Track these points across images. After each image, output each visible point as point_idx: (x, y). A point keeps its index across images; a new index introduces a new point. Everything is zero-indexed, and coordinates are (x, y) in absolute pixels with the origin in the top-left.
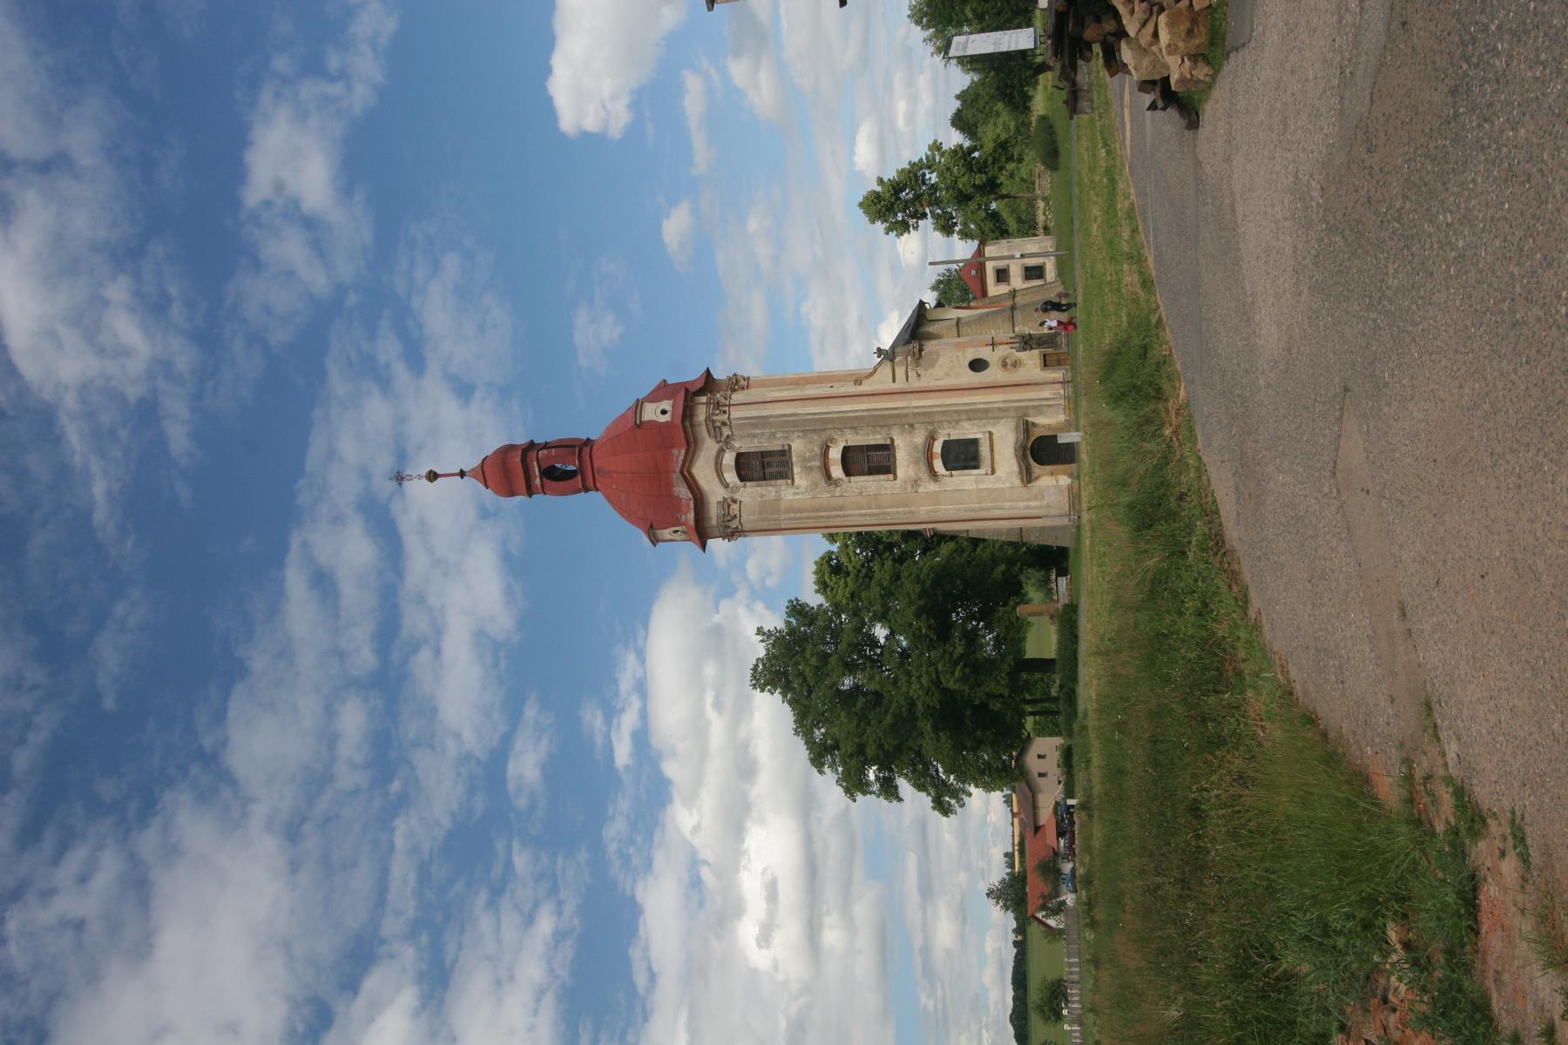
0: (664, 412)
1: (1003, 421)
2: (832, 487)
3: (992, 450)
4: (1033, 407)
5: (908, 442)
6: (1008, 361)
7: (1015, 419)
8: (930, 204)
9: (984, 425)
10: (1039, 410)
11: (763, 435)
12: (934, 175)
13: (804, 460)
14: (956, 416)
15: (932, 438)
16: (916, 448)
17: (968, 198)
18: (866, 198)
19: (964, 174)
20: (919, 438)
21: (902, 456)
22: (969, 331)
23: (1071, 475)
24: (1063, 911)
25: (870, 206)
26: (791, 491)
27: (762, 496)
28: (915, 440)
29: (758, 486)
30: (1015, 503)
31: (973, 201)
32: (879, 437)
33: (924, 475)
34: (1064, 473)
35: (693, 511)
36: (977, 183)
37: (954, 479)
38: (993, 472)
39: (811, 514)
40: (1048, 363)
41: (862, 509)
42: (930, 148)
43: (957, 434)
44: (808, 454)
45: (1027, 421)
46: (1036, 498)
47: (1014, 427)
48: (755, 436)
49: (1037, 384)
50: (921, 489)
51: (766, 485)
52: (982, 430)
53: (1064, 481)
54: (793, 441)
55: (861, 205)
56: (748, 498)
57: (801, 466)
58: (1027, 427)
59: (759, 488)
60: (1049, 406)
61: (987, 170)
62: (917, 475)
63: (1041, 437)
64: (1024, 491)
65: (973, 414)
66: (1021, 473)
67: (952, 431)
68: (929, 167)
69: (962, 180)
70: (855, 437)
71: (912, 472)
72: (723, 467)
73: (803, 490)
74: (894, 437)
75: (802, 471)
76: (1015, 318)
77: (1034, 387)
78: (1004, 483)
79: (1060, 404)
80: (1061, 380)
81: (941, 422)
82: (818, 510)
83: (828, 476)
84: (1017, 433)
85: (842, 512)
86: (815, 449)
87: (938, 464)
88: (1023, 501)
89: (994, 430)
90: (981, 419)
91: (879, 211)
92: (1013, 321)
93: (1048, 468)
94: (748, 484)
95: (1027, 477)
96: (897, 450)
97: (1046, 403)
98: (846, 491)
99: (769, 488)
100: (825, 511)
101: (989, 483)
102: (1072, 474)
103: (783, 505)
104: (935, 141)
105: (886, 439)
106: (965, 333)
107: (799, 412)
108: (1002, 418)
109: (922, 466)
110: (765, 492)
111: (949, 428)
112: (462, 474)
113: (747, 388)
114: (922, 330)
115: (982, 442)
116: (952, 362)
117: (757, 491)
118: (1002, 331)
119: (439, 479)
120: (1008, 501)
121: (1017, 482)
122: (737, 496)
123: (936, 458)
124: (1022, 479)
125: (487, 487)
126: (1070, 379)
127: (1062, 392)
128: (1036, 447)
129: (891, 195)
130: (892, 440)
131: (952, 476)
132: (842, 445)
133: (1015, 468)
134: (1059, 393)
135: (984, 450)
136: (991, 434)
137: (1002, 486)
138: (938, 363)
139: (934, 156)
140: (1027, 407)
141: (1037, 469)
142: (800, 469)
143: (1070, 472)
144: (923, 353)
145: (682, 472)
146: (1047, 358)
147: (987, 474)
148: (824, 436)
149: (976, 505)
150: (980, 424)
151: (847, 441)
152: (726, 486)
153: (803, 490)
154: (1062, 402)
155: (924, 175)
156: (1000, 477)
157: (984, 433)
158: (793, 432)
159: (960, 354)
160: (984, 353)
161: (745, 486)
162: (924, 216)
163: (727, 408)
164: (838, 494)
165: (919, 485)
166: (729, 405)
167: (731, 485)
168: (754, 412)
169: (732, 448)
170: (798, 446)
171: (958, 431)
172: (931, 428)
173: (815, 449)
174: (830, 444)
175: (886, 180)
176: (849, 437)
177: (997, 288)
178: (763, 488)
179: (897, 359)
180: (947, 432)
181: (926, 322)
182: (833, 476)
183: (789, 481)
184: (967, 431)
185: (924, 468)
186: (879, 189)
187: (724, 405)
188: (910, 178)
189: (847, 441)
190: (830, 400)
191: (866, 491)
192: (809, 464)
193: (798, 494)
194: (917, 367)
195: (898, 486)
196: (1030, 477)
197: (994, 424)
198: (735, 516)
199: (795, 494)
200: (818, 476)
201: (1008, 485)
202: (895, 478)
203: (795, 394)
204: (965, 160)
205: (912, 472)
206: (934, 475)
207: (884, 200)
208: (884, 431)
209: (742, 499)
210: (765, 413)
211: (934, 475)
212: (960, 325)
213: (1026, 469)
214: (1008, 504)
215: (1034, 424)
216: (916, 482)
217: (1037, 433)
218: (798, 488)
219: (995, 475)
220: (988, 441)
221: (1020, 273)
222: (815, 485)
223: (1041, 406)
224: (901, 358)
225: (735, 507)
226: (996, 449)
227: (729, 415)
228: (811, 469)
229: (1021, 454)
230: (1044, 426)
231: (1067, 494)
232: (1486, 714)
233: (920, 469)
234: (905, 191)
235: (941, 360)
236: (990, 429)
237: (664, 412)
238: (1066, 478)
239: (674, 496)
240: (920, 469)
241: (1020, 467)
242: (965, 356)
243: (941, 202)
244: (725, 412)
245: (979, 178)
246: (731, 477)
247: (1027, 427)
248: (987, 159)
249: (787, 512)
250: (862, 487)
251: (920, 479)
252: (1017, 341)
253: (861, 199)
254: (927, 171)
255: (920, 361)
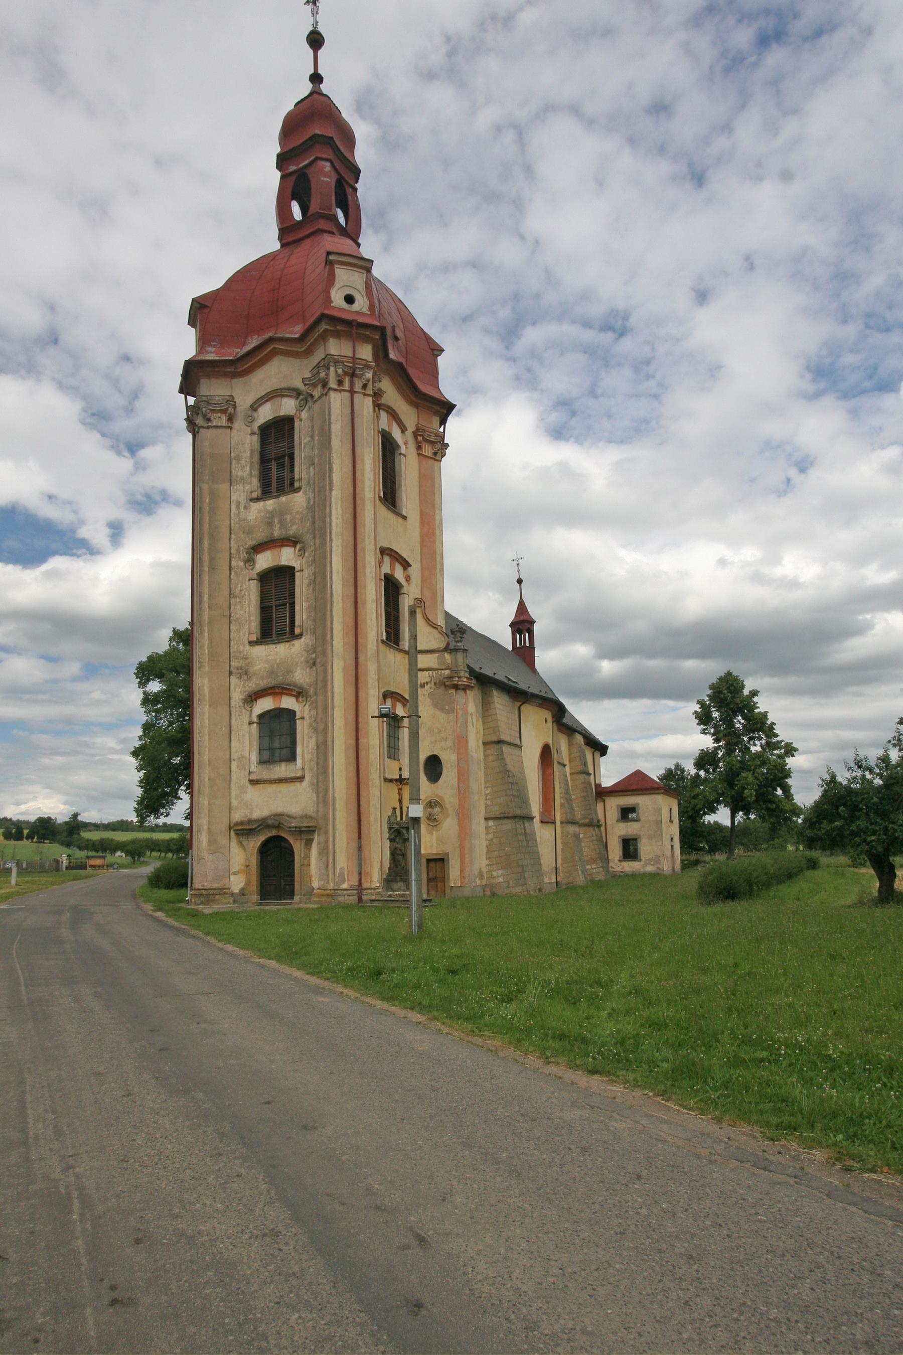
0: (350, 299)
1: (315, 795)
2: (244, 555)
3: (280, 781)
4: (327, 842)
5: (297, 660)
6: (437, 810)
7: (314, 815)
8: (727, 744)
9: (311, 769)
10: (324, 851)
11: (312, 449)
12: (759, 749)
13: (281, 513)
14: (321, 726)
15: (299, 693)
16: (290, 671)
17: (731, 785)
18: (736, 679)
19: (756, 778)
20: (301, 676)
21: (281, 651)
22: (491, 758)
23: (242, 893)
24: (133, 858)
25: (727, 682)
26: (243, 499)
27: (238, 458)
28: (299, 671)
29: (252, 452)
30: (206, 811)
31: (728, 788)
32: (304, 617)
33: (254, 685)
34: (248, 883)
35: (218, 358)
36: (746, 791)
37: (246, 727)
38: (254, 782)
39: (206, 526)
40: (432, 864)
41: (210, 596)
42: (788, 745)
43: (302, 728)
44: (288, 517)
45: (314, 831)
46: (212, 841)
47: (309, 814)
48: (312, 437)
49: (360, 848)
50: (234, 680)
51: (252, 463)
52: (306, 767)
53: (237, 883)
54: (305, 493)
55: (729, 674)
56: (236, 438)
57: (274, 509)
58: (307, 832)
59: (248, 454)
60: (327, 866)
61: (761, 803)
62: (255, 674)
63: (293, 852)
64: (224, 826)
65: (323, 750)
66: (250, 821)
67: (307, 722)
68: (768, 744)
69: (750, 776)
70: (306, 581)
71: (259, 667)
72: (279, 399)
73: (242, 515)
74: (303, 639)
75: (268, 511)
76: (506, 821)
77: (354, 845)
78: (237, 797)
79: (328, 882)
80: (365, 885)
81: (316, 708)
82: (211, 536)
83: (258, 548)
84: (302, 817)
85: (206, 569)
86: (294, 527)
87: (265, 704)
88: (209, 822)
89: (306, 783)
90: (318, 764)
91: (720, 692)
92: (500, 818)
93: (254, 861)
94: (256, 438)
95: (244, 830)
96: (287, 645)
97: (331, 861)
98: (237, 574)
99: (248, 469)
100: (210, 544)
101: (239, 777)
102: (243, 895)
103: (224, 487)
104: (796, 750)
105: (301, 626)
106: (489, 752)
107: (334, 493)
108: (318, 797)
109: (265, 681)
110: (243, 462)
111: (310, 718)
112: (316, 78)
113: (419, 454)
114: (495, 693)
115: (291, 766)
116: (440, 732)
117: (245, 451)
118: (489, 802)
119: (311, 52)
120: (209, 804)
121: (237, 817)
122: (238, 424)
123: (274, 701)
124: (241, 823)
125: (295, 106)
126: (364, 898)
127: (345, 886)
128: (283, 844)
129: (738, 704)
130: (300, 636)
131: (250, 723)
132: (296, 564)
133: (257, 814)
134: (343, 881)
135: (282, 770)
136: (301, 779)
137: (233, 794)
138: (438, 713)
139: (781, 748)
140: (326, 833)
141: (255, 843)
142: (270, 508)
143: (246, 892)
144: (453, 691)
145: (271, 340)
146: (439, 864)
147: (250, 773)
148: (308, 537)
149: (206, 758)
150: (312, 763)
151: (302, 571)
152: (254, 407)
153: (242, 515)
154: (332, 885)
155: (760, 739)
156: (246, 792)
157: (303, 769)
158: (314, 492)
159: (449, 743)
160: (449, 774)
161: (252, 434)
162: (717, 741)
163: (347, 385)
164: (234, 563)
165: (240, 678)
166: (352, 392)
167: (255, 415)
168: (338, 428)
169: (300, 408)
170: (298, 501)
171: (306, 731)
172: (311, 691)
173: (294, 527)
174: (298, 547)
175: (755, 699)
176: (306, 573)
177: (615, 808)
178: (248, 460)
179: (447, 656)
180: (306, 716)
181: (519, 704)
182: (259, 556)
183: (255, 495)
184: (305, 747)
185: (263, 684)
186: (746, 692)
187: (352, 384)
188: (757, 723)
189: (302, 571)
190: (351, 539)
191: (236, 605)
192: (276, 521)
193: (238, 507)
194: (435, 684)
195: (241, 648)
196: (242, 834)
197: (312, 784)
198: (209, 420)
199: (238, 504)
200: (260, 536)
201: (234, 803)
202: (251, 643)
203: (367, 489)
204: (773, 780)
205: (259, 667)
206: (253, 697)
207: (733, 697)
208: (309, 624)
209: (234, 432)
210: (336, 443)
211: (253, 697)
212: (498, 746)
213: (251, 830)
214: (206, 802)
215: (309, 843)
216: (244, 673)
217: (298, 847)
218: (245, 507)
219: (249, 786)
220: (293, 775)
221: (630, 833)
222: (248, 532)
223: (327, 853)
224: (449, 661)
225: (224, 421)
226: (283, 788)
227: (335, 390)
228: (270, 524)
229: (270, 822)
230: (308, 856)
231: (215, 886)
232: (410, 1124)
233: (262, 678)
234: (743, 719)
235: (442, 716)
236: (307, 778)
237: (350, 299)
238: (242, 885)
239: (246, 337)
240: (262, 678)
241: (256, 821)
242: (446, 749)
243: (729, 755)
244: (340, 383)
245: (751, 795)
246: (266, 413)
247: (307, 832)
248: (774, 802)
249: (212, 493)
250: (242, 597)
251: (249, 679)
252: (404, 819)
253: (735, 674)
254: (763, 742)
255: (442, 688)
